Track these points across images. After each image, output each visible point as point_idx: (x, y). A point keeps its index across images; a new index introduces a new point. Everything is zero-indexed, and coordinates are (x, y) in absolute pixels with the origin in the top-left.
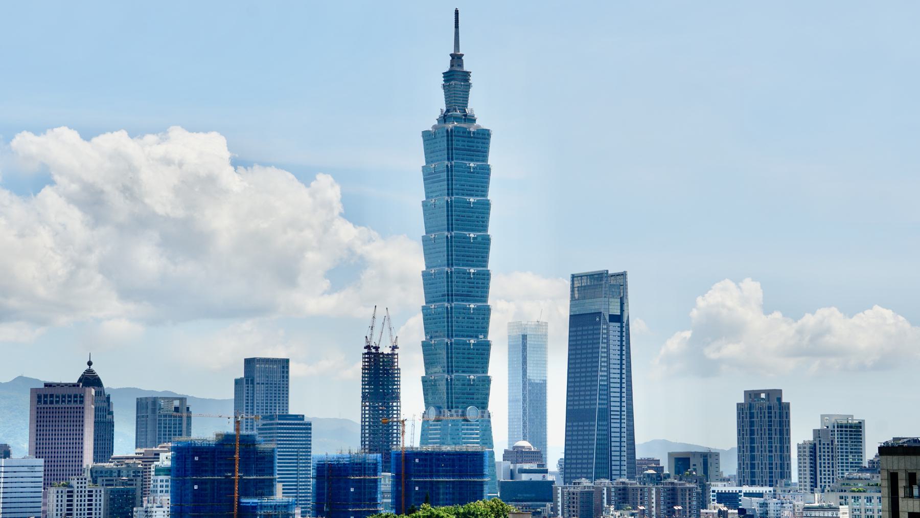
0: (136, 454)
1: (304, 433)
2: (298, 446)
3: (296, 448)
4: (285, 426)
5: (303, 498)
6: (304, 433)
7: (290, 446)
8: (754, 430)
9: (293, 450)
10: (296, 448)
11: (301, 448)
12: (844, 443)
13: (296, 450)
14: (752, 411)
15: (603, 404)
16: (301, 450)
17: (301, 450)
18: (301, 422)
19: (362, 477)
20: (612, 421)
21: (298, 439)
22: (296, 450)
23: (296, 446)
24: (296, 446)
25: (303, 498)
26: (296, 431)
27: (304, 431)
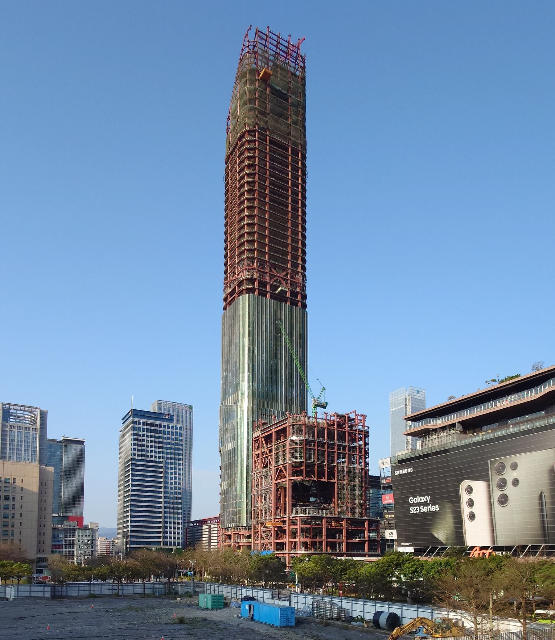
18: (166, 424)
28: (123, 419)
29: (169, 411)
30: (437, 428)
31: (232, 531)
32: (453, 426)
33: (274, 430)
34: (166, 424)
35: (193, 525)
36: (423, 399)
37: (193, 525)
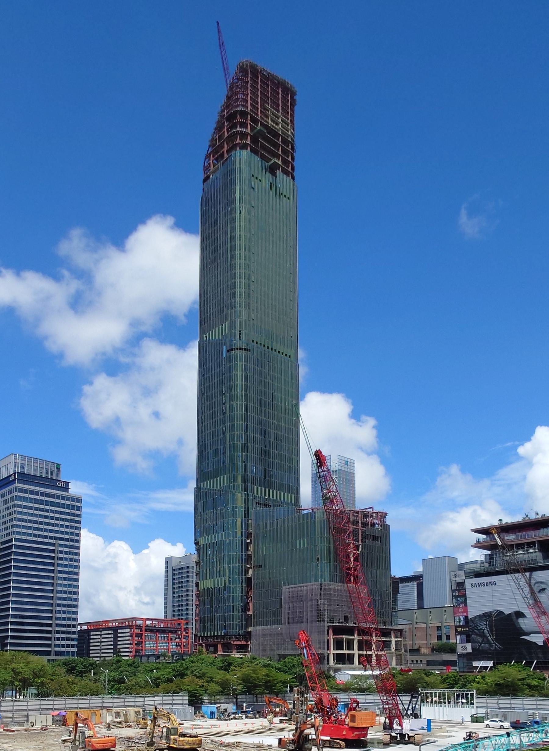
1: (68, 514)
3: (51, 538)
4: (42, 498)
6: (68, 514)
10: (51, 538)
11: (61, 539)
29: (47, 473)
32: (531, 545)
36: (352, 471)
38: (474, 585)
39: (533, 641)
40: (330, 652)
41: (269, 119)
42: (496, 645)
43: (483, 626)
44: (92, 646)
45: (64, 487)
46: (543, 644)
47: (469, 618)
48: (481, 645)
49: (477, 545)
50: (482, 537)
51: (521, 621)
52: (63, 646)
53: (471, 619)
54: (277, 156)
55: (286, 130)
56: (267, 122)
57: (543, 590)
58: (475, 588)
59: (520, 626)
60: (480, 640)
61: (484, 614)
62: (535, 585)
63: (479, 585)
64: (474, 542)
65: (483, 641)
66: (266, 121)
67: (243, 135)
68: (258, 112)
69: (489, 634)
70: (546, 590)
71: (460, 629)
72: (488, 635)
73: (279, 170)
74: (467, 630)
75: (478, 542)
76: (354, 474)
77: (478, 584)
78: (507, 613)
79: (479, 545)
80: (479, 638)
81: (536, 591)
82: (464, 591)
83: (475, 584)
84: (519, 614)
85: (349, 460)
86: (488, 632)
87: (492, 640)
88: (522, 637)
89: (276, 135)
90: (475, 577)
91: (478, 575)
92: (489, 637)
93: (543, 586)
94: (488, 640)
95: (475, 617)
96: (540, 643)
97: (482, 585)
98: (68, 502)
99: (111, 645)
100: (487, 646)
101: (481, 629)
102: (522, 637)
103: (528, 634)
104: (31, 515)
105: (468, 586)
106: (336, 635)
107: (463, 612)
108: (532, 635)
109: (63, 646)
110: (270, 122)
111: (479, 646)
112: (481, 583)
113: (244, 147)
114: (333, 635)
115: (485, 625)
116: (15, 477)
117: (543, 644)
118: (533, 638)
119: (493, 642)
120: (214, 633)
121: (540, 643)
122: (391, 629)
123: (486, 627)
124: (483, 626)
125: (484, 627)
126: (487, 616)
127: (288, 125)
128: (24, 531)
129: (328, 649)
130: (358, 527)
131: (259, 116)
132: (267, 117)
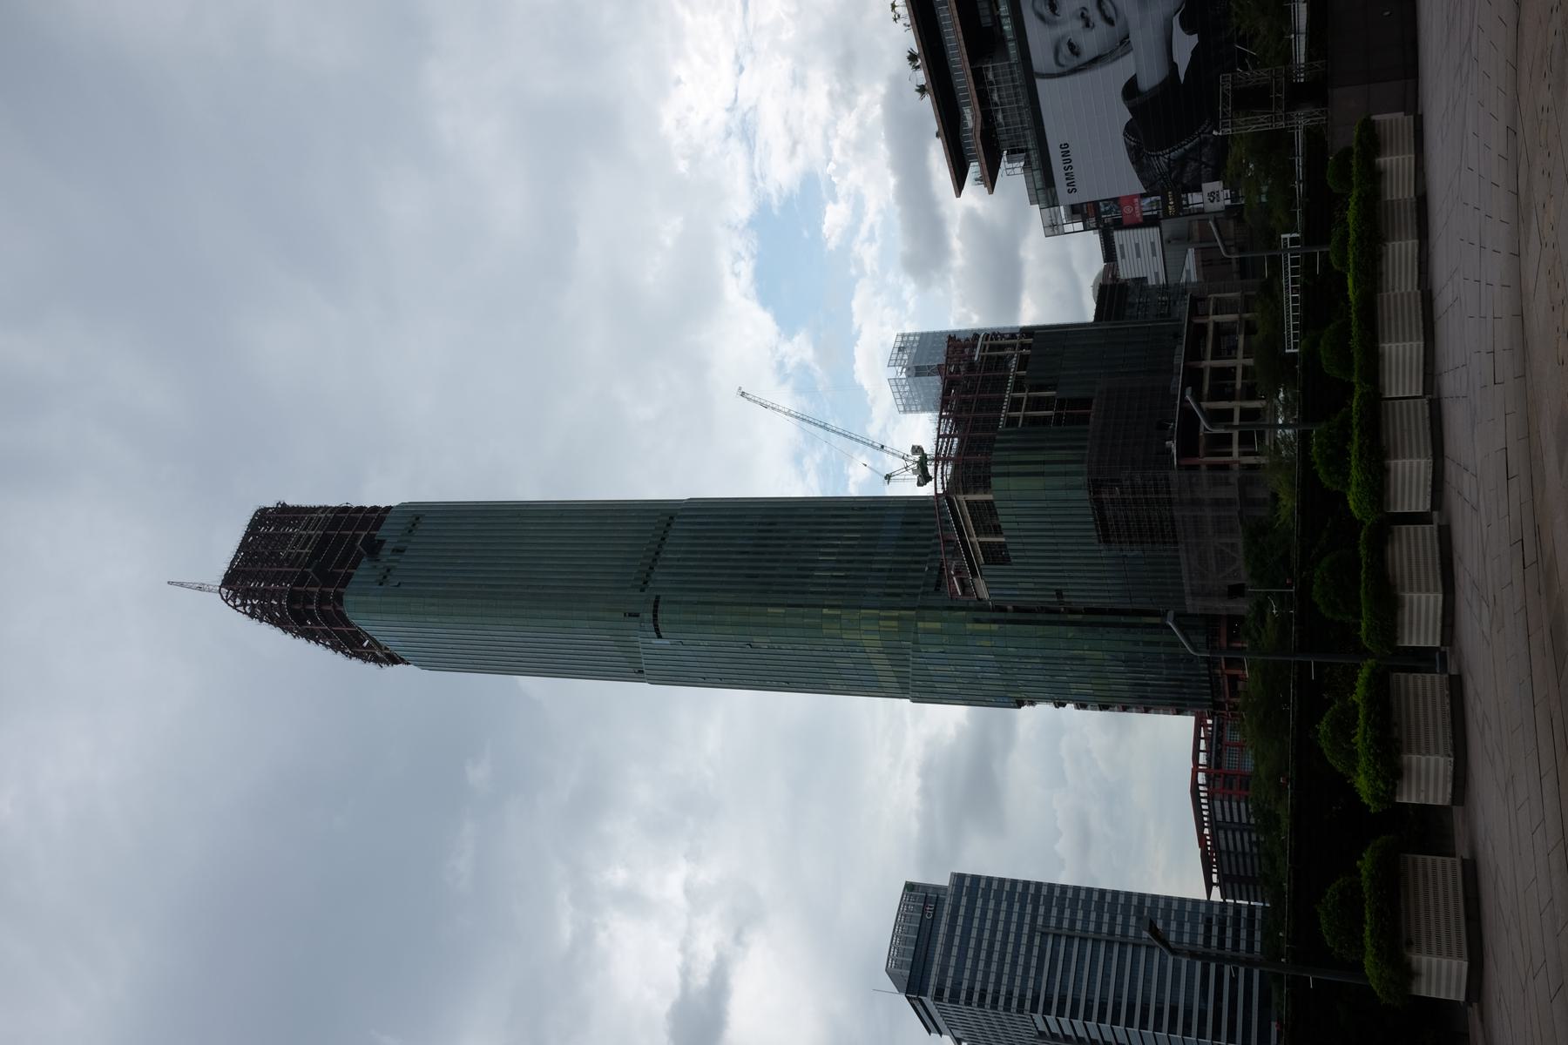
0: (1154, 254)
1: (986, 902)
2: (1026, 929)
5: (1243, 934)
6: (986, 902)
7: (1008, 959)
8: (1201, 371)
9: (1035, 951)
12: (1003, 85)
13: (1037, 941)
14: (1141, 220)
15: (1255, 891)
16: (1040, 921)
17: (1040, 921)
18: (947, 909)
19: (1363, 625)
20: (1093, 526)
21: (1010, 948)
22: (1037, 941)
23: (1024, 940)
24: (1024, 940)
25: (1243, 934)
26: (974, 933)
27: (980, 902)
28: (929, 1032)
30: (972, 69)
31: (1219, 671)
32: (978, 77)
33: (974, 539)
34: (947, 909)
35: (1215, 873)
36: (917, 338)
37: (1215, 873)
38: (1071, 188)
39: (1189, 55)
40: (1235, 462)
41: (302, 553)
42: (1203, 132)
43: (1162, 161)
44: (1246, 871)
45: (935, 907)
46: (1196, 35)
47: (1145, 191)
48: (1204, 163)
49: (989, 184)
50: (974, 170)
51: (1145, 84)
52: (1251, 934)
53: (1146, 189)
54: (356, 537)
55: (319, 521)
56: (305, 557)
57: (1071, 46)
58: (1078, 185)
59: (1156, 87)
60: (1193, 165)
61: (1133, 163)
62: (1062, 66)
63: (1069, 177)
64: (983, 189)
65: (1196, 161)
66: (305, 557)
67: (323, 599)
68: (291, 572)
69: (1179, 148)
70: (1072, 41)
71: (1170, 208)
72: (1180, 150)
73: (375, 535)
74: (1173, 194)
75: (981, 181)
76: (922, 335)
77: (1067, 179)
78: (1129, 117)
79: (990, 179)
80: (1188, 169)
81: (1076, 62)
82: (1085, 206)
83: (1068, 185)
84: (1131, 90)
85: (898, 345)
86: (1173, 151)
87: (1192, 141)
88: (1182, 78)
89: (325, 539)
90: (1054, 186)
91: (1049, 181)
92: (1187, 147)
93: (1065, 49)
94: (1191, 149)
95: (1142, 179)
96: (1194, 40)
97: (1069, 171)
98: (964, 901)
99: (1238, 872)
100: (1205, 150)
101: (1168, 165)
102: (1182, 78)
103: (1173, 67)
104: (995, 922)
105: (1076, 199)
106: (1211, 374)
107: (1133, 205)
108: (1176, 59)
109: (1251, 934)
110: (306, 550)
111: (1207, 166)
112: (1066, 174)
113: (339, 598)
114: (1198, 456)
115: (1158, 158)
116: (914, 998)
117: (1196, 35)
118: (1183, 58)
119: (1197, 139)
120: (1205, 681)
121: (1194, 40)
122: (1190, 322)
123: (1163, 156)
124: (1162, 161)
125: (1163, 161)
126: (1137, 156)
127: (312, 519)
128: (1023, 950)
129: (1225, 467)
130: (980, 378)
131: (297, 570)
132: (299, 555)
